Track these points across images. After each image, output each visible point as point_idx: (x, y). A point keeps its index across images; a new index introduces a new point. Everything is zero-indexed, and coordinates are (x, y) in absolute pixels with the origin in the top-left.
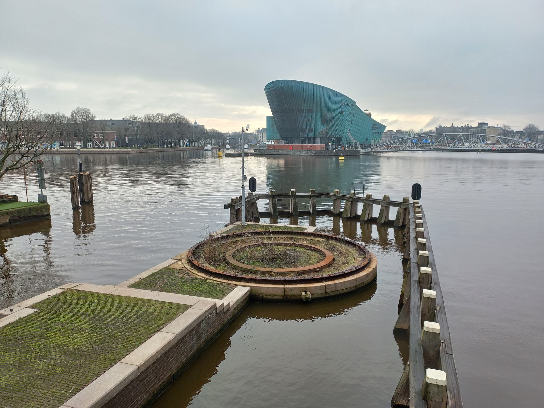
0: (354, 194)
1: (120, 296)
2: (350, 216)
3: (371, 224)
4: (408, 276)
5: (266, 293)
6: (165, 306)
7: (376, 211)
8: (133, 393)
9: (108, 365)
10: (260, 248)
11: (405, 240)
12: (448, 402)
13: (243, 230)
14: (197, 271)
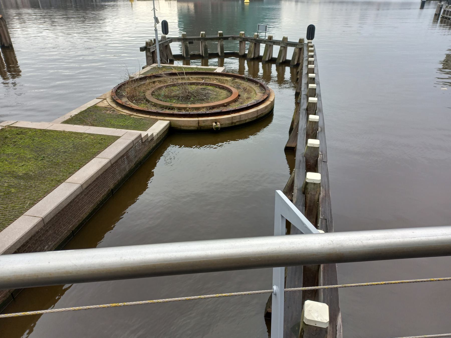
0: (258, 35)
1: (55, 131)
2: (254, 57)
3: (271, 64)
4: (298, 106)
5: (183, 125)
6: (97, 138)
7: (276, 51)
8: (80, 204)
9: (55, 185)
10: (176, 88)
11: (299, 77)
12: (321, 194)
13: (159, 72)
14: (121, 108)
